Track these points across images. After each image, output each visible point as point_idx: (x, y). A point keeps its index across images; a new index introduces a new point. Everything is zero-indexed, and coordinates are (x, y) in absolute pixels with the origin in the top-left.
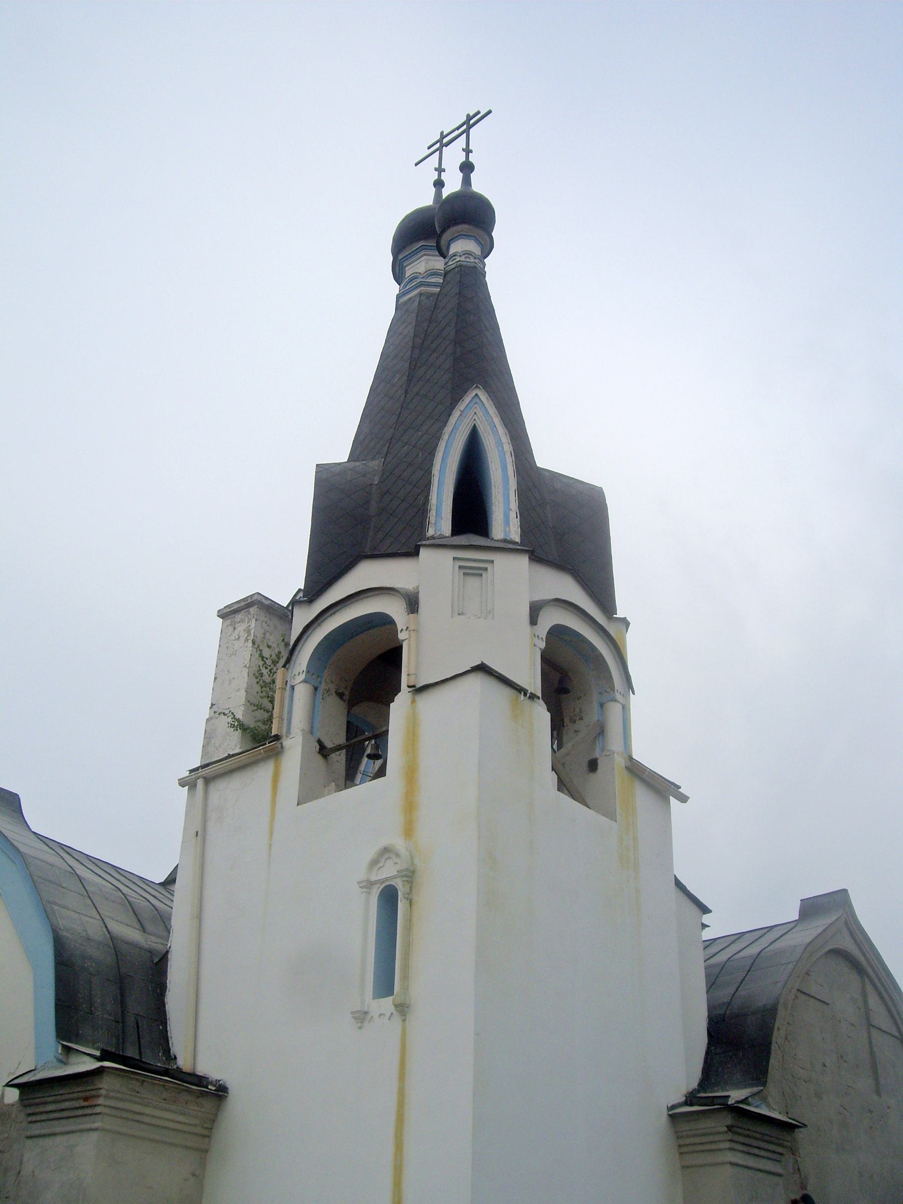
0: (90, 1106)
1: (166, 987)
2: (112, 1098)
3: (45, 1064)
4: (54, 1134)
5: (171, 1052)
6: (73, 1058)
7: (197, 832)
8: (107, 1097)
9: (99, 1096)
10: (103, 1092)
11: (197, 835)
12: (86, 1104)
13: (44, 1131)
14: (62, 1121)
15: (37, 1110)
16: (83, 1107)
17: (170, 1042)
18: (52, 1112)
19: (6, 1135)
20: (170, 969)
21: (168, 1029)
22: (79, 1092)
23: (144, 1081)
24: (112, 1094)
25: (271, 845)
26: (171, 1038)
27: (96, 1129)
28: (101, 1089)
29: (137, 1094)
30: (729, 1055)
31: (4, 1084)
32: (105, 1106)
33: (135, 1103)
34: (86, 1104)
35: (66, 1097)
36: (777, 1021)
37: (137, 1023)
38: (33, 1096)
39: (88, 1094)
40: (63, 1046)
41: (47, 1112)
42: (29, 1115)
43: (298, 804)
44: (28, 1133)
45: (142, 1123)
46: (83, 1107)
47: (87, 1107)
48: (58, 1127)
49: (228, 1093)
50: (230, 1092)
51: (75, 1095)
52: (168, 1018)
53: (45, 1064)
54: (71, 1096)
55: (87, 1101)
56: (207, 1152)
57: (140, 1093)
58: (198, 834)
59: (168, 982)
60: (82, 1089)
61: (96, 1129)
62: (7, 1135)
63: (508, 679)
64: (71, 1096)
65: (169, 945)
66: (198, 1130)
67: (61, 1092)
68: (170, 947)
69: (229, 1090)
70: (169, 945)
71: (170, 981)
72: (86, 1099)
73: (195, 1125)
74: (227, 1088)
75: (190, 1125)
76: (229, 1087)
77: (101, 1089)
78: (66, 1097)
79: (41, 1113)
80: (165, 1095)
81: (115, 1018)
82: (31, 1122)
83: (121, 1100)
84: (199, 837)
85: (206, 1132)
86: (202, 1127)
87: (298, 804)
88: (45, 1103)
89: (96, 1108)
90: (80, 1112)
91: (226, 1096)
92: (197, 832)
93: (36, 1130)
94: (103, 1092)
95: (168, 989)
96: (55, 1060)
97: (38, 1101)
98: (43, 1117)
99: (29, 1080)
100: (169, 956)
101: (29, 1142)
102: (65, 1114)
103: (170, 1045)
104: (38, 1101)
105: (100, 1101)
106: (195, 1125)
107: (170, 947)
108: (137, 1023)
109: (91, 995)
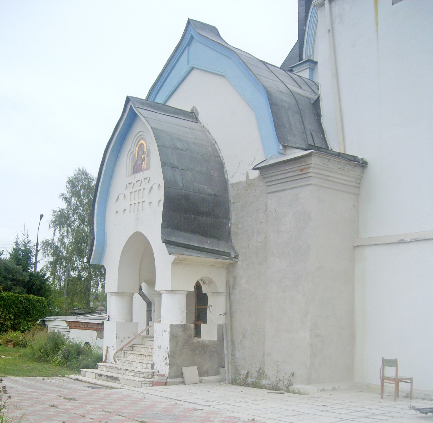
0: (305, 174)
1: (321, 115)
2: (317, 168)
3: (272, 156)
4: (285, 190)
5: (329, 148)
6: (289, 151)
7: (329, 30)
8: (314, 168)
9: (309, 168)
10: (312, 165)
11: (329, 32)
12: (302, 173)
13: (277, 189)
14: (282, 184)
15: (271, 179)
16: (300, 175)
17: (328, 143)
18: (281, 179)
19: (254, 194)
20: (322, 105)
21: (326, 136)
22: (298, 167)
23: (330, 159)
24: (316, 166)
25: (377, 30)
26: (328, 141)
27: (310, 185)
28: (311, 164)
29: (327, 166)
30: (51, 278)
31: (252, 168)
32: (314, 173)
33: (326, 170)
34: (302, 173)
35: (289, 170)
36: (173, 241)
37: (311, 134)
38: (272, 172)
39: (303, 167)
40: (282, 145)
41: (278, 180)
42: (267, 182)
43: (393, 4)
44: (269, 191)
45: (330, 181)
46: (300, 175)
47: (303, 174)
48: (286, 186)
49: (367, 165)
50: (368, 164)
51: (296, 169)
52: (324, 131)
53: (272, 156)
54: (293, 169)
55: (302, 171)
56: (359, 195)
57: (328, 165)
58: (330, 31)
59: (321, 112)
60: (300, 165)
61: (310, 185)
62: (254, 194)
63: (102, 160)
64: (293, 169)
65: (319, 93)
66: (354, 184)
67: (286, 168)
68: (320, 94)
69: (368, 163)
70: (319, 93)
71: (323, 112)
72: (302, 170)
73: (353, 182)
74: (367, 162)
75: (350, 181)
76: (368, 161)
77: (311, 164)
78: (289, 170)
79: (275, 180)
80: (339, 166)
81: (302, 131)
82: (268, 186)
83: (320, 169)
84: (330, 33)
85: (358, 185)
86: (356, 183)
87: (393, 4)
88: (276, 175)
89: (308, 174)
90: (299, 177)
91: (368, 166)
92: (329, 30)
93: (271, 189)
94: (312, 165)
95: (322, 116)
96: (277, 154)
97: (272, 174)
98: (276, 182)
99: (267, 164)
100: (320, 99)
101: (269, 196)
102: (288, 180)
103: (328, 144)
104: (272, 174)
105: (311, 170)
106: (353, 182)
107: (320, 94)
108: (311, 134)
109: (289, 120)
